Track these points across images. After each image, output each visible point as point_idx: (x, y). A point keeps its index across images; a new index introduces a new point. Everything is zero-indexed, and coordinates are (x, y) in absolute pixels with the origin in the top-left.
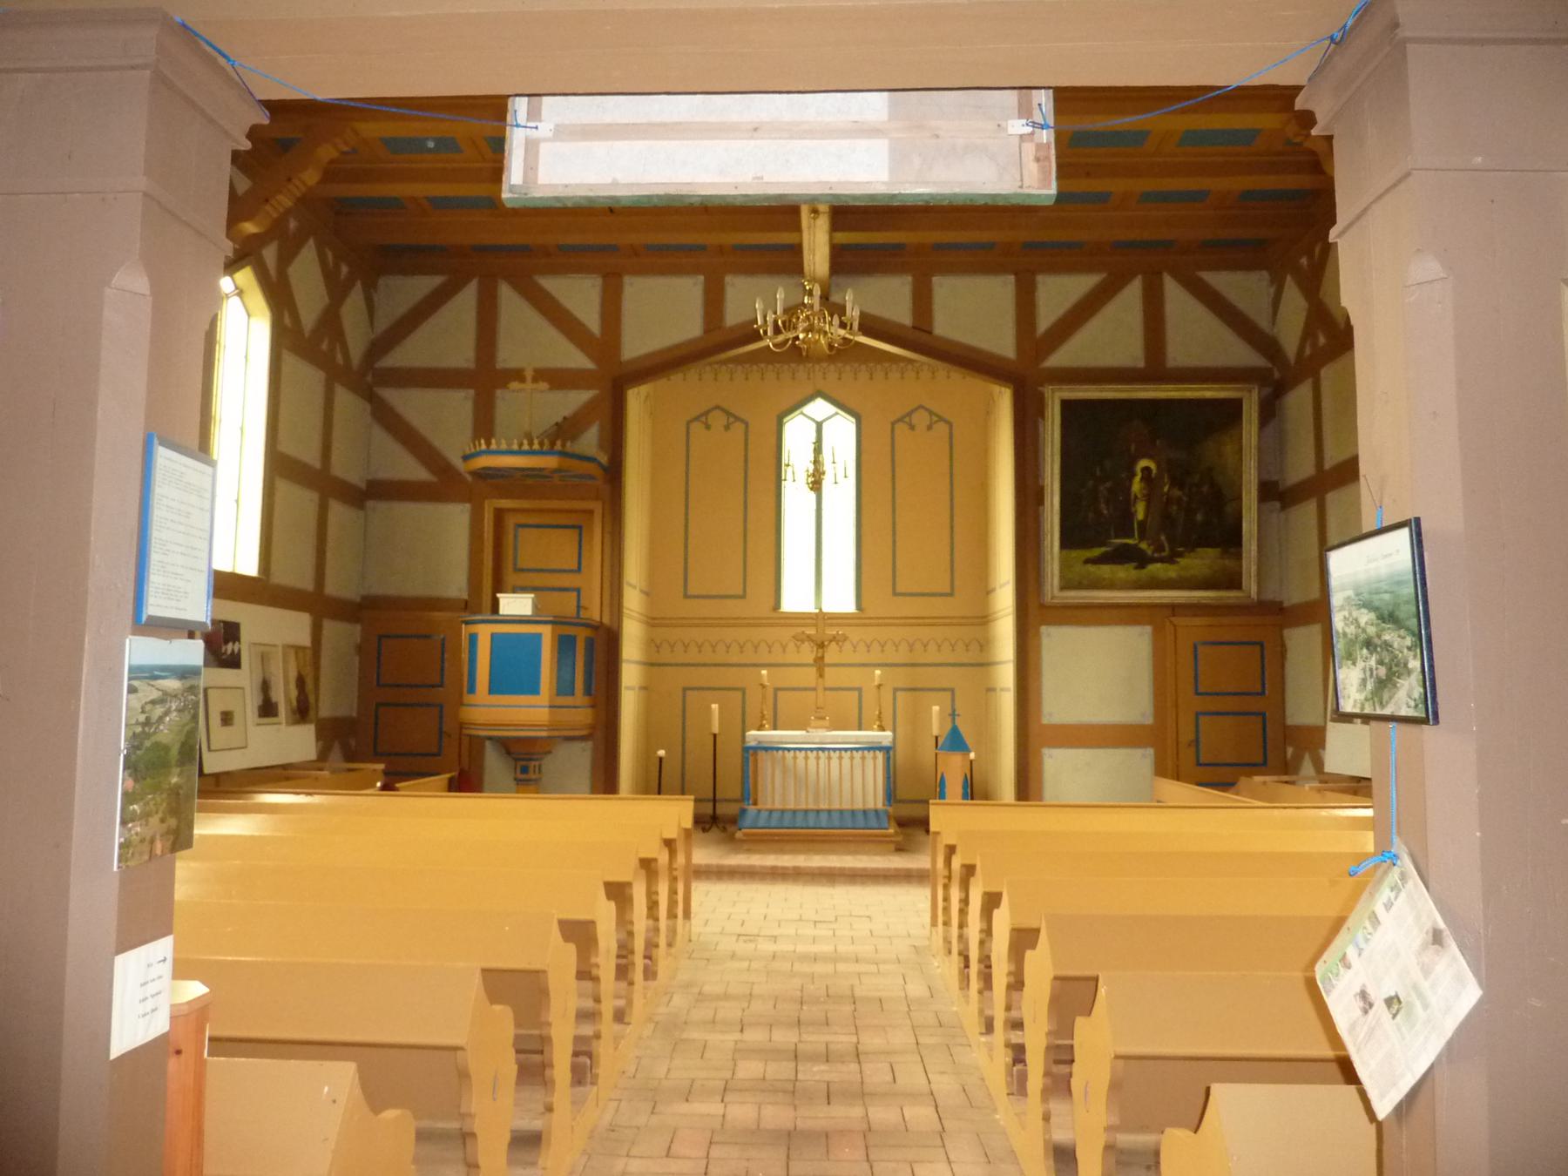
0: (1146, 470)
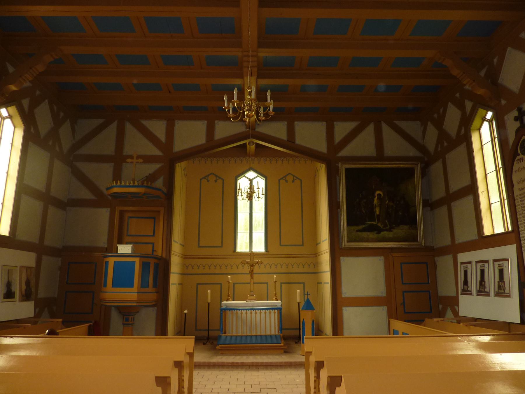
0: (379, 195)
